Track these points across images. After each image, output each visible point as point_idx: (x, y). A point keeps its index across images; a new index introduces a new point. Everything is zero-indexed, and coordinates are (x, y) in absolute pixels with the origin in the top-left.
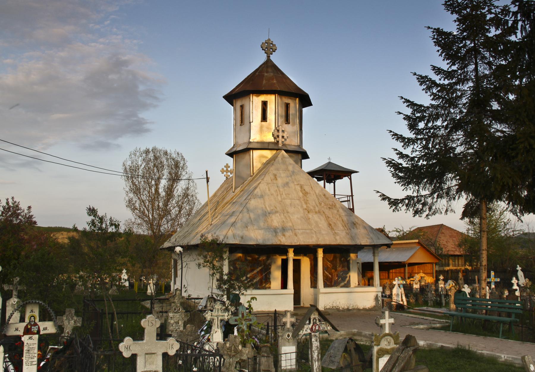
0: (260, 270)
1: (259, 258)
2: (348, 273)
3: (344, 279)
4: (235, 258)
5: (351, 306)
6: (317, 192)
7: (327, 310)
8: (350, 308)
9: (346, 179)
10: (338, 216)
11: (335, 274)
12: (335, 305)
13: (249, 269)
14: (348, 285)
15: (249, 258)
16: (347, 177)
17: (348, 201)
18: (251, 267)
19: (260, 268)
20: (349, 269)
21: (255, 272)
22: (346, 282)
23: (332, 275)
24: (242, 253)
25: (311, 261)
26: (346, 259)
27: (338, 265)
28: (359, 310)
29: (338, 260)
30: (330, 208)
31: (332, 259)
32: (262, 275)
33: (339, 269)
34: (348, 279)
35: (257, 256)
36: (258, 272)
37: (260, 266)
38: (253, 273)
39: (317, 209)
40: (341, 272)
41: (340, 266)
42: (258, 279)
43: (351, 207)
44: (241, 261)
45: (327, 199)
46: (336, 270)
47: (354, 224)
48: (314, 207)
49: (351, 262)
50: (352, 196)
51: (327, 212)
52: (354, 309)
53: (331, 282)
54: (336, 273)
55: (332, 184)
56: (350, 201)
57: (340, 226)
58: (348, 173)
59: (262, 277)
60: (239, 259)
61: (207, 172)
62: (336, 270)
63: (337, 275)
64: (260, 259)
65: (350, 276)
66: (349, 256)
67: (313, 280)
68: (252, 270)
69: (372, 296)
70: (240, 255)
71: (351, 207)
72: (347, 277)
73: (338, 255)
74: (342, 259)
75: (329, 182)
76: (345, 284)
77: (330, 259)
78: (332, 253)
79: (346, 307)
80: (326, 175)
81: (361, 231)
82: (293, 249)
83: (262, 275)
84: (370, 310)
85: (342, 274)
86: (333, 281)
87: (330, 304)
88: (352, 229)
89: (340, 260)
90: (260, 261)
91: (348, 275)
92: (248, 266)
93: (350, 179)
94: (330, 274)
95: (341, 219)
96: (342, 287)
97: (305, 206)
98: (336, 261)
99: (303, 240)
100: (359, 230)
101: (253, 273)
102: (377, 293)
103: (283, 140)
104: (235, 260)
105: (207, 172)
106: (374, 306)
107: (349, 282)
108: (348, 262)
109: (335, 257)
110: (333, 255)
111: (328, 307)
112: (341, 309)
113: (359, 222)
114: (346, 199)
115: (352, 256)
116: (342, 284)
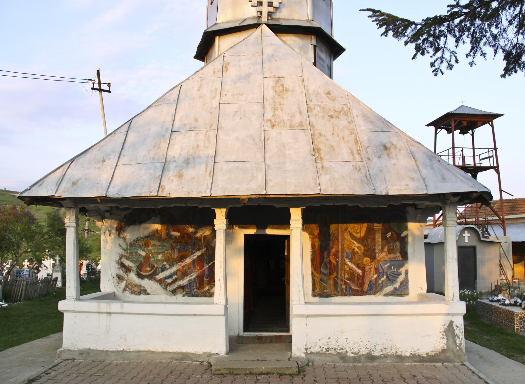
0: (199, 257)
1: (195, 233)
2: (402, 266)
3: (392, 278)
4: (146, 233)
5: (379, 348)
6: (312, 88)
7: (312, 357)
8: (376, 354)
9: (487, 127)
10: (347, 132)
11: (371, 267)
12: (333, 344)
13: (176, 255)
14: (402, 291)
15: (177, 234)
16: (487, 124)
17: (489, 157)
18: (179, 250)
19: (198, 253)
20: (405, 256)
21: (188, 261)
22: (397, 285)
23: (363, 270)
24: (162, 223)
25: (312, 239)
26: (399, 235)
27: (378, 248)
28: (400, 358)
29: (378, 237)
30: (331, 117)
31: (362, 234)
32: (202, 267)
33: (381, 256)
34: (401, 278)
35: (191, 230)
36: (194, 261)
37: (199, 250)
38: (183, 264)
39: (297, 119)
40: (386, 262)
41: (382, 250)
42: (194, 276)
43: (495, 165)
44: (160, 239)
45: (334, 99)
46: (373, 258)
47: (385, 148)
48: (292, 116)
49: (410, 239)
50: (495, 149)
51: (322, 125)
52: (386, 356)
53: (362, 285)
54: (373, 265)
55: (468, 136)
56: (493, 156)
57: (346, 155)
58: (488, 118)
59: (204, 272)
60: (154, 235)
61: (98, 72)
62: (373, 258)
63: (377, 270)
64: (198, 235)
65: (407, 273)
66: (406, 228)
67: (317, 280)
68: (182, 258)
69: (439, 324)
70: (157, 227)
71: (495, 165)
72: (400, 274)
73: (378, 226)
74: (389, 235)
75: (463, 132)
76: (396, 289)
77: (358, 235)
78: (363, 222)
79: (364, 352)
80: (455, 121)
81: (402, 161)
82: (224, 210)
83: (202, 267)
84: (431, 358)
85: (390, 267)
86: (367, 282)
87: (320, 343)
88: (375, 160)
89: (384, 237)
90: (199, 239)
91: (403, 270)
92: (173, 248)
93: (492, 126)
94: (358, 267)
95: (352, 138)
96: (386, 295)
97: (269, 115)
98: (374, 239)
99: (246, 186)
100: (393, 161)
101: (183, 264)
102: (450, 318)
103: (271, 9)
104: (147, 237)
105: (98, 72)
106: (443, 351)
107: (405, 284)
108: (404, 242)
109: (370, 232)
110: (365, 225)
111: (315, 349)
112: (350, 354)
113: (400, 144)
114: (487, 155)
115: (413, 227)
116: (389, 289)
